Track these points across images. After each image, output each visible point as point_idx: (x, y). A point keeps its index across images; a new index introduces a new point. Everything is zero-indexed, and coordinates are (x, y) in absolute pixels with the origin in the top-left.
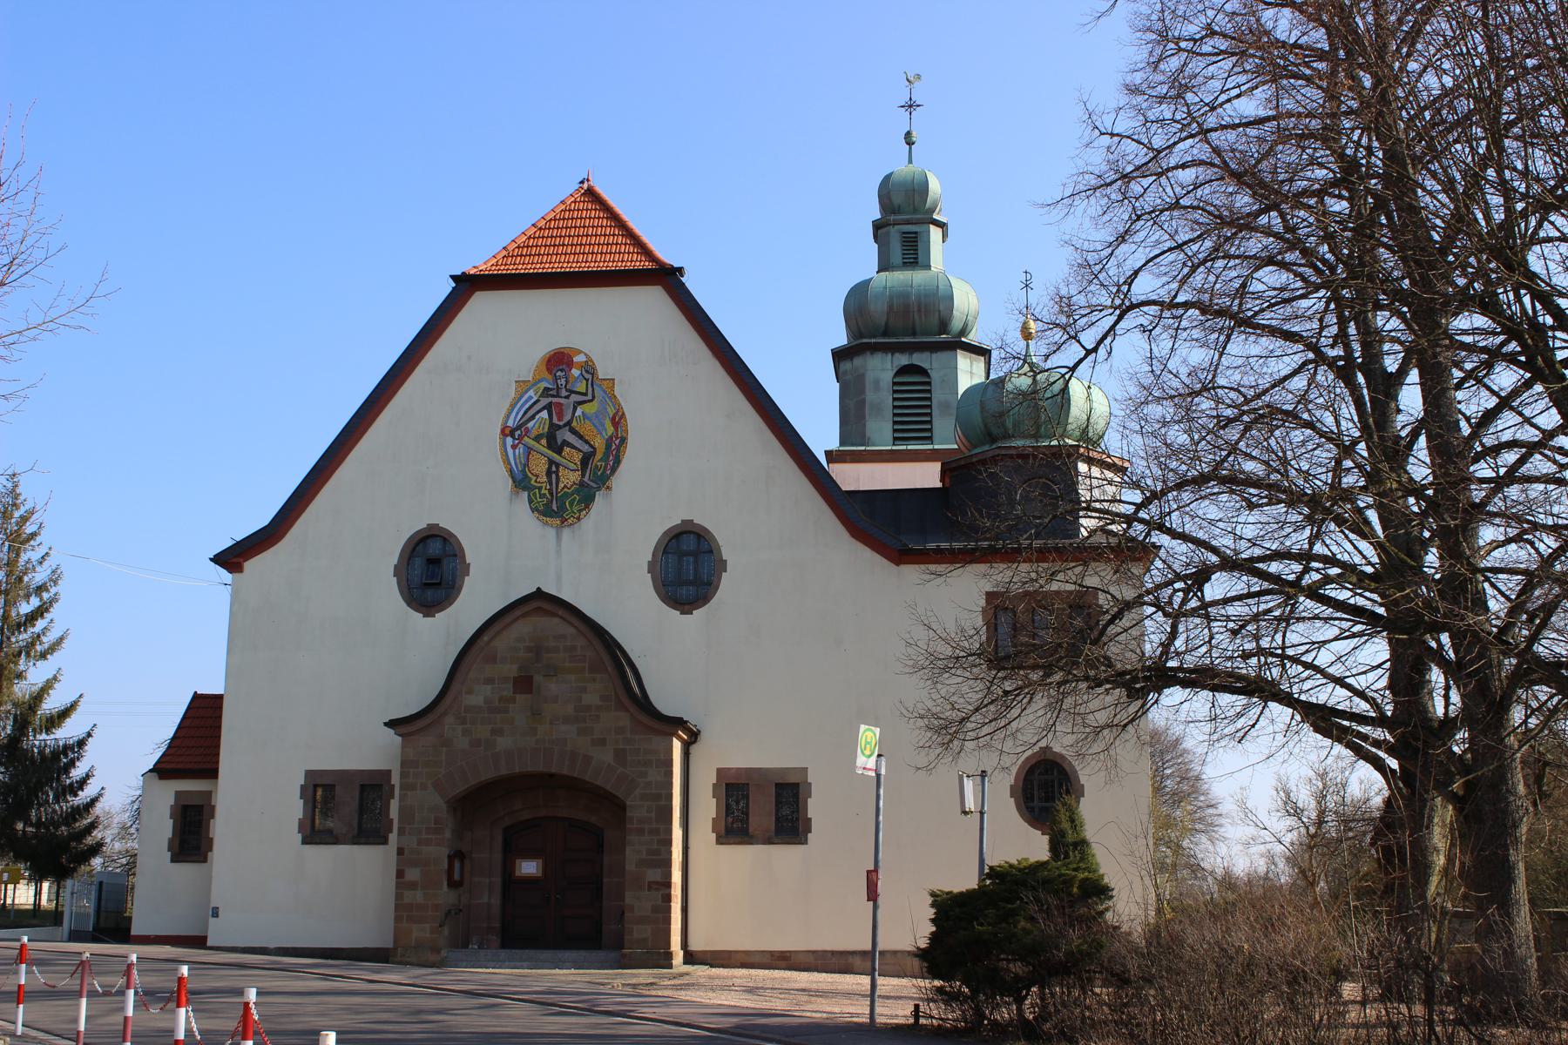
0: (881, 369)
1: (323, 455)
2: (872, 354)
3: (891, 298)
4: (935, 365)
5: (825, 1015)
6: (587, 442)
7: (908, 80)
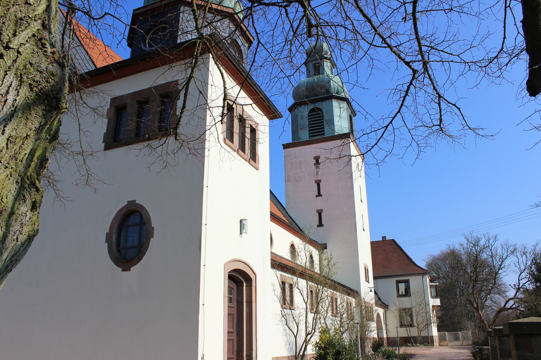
0: (304, 111)
1: (354, 208)
2: (300, 106)
3: (307, 85)
4: (324, 106)
5: (221, 68)
6: (182, 113)
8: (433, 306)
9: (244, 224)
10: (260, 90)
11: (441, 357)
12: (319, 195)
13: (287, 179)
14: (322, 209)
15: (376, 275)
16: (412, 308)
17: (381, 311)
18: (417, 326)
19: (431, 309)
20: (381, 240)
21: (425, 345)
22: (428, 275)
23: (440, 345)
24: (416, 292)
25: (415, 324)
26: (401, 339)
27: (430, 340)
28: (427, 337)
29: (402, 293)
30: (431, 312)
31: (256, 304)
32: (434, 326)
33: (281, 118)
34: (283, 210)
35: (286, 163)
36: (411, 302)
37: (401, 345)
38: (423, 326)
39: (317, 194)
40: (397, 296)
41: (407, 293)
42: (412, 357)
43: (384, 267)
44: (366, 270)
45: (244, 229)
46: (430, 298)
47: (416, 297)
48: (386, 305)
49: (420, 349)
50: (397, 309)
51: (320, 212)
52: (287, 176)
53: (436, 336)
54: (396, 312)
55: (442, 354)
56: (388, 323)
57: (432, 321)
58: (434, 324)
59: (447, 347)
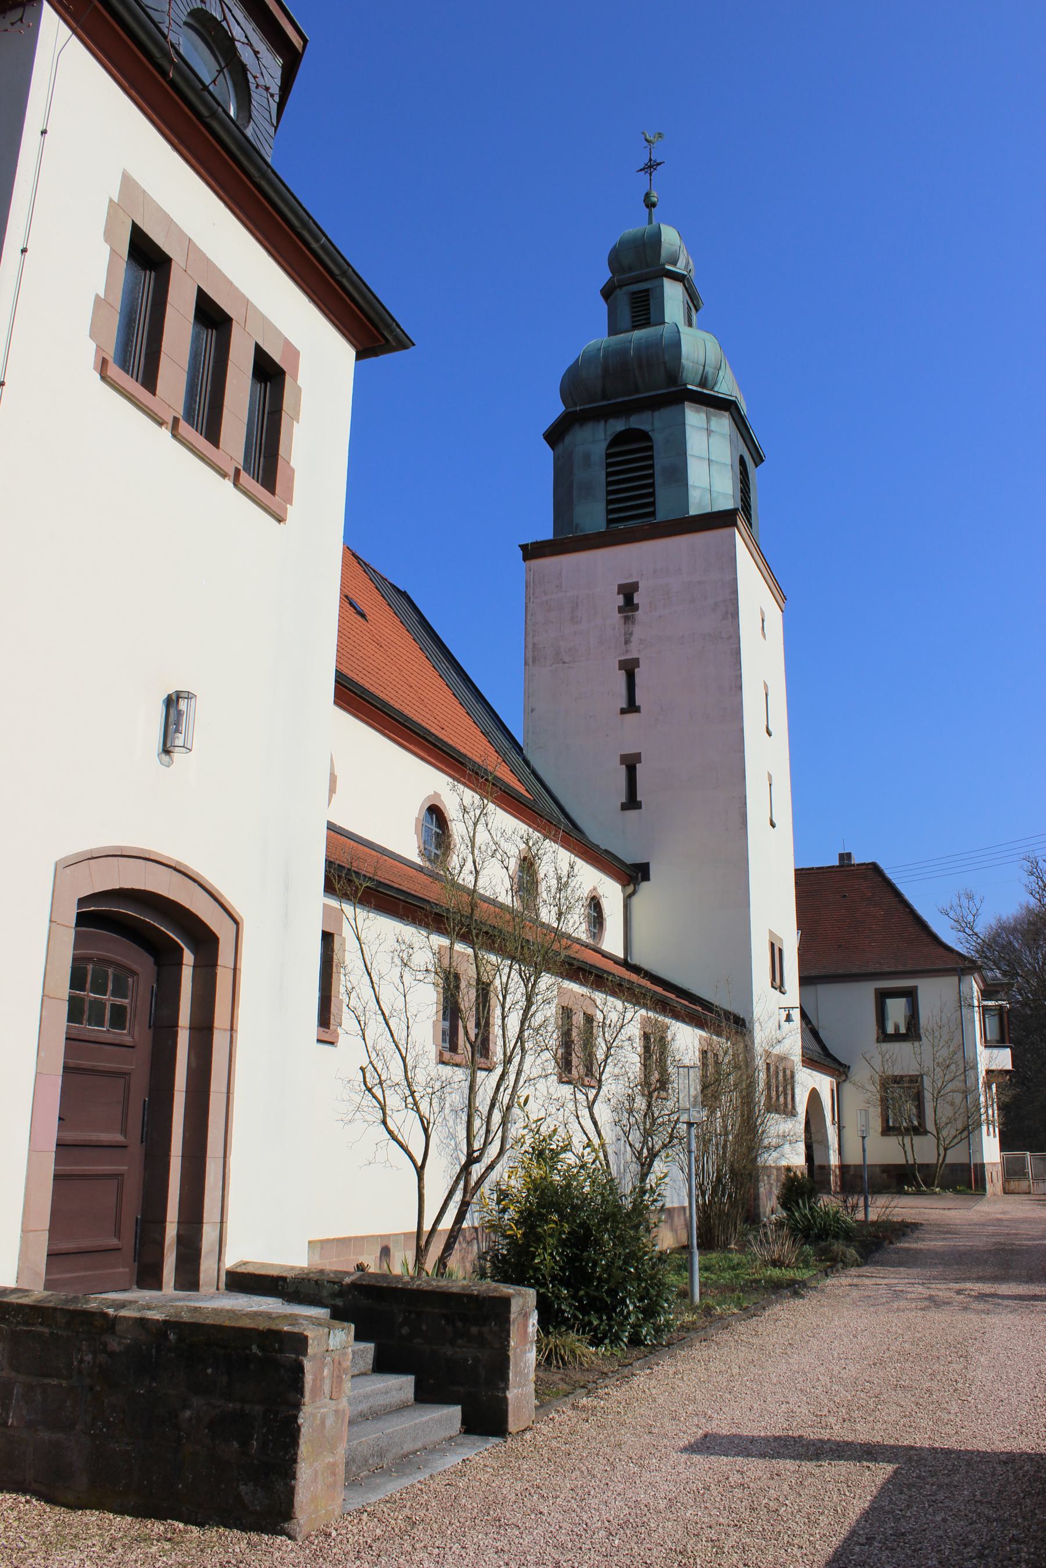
2: (581, 425)
3: (606, 357)
4: (657, 425)
7: (647, 140)
8: (989, 1072)
9: (179, 713)
10: (301, 212)
11: (998, 1235)
12: (632, 707)
13: (530, 654)
14: (640, 753)
16: (921, 1076)
17: (824, 1083)
18: (935, 1132)
19: (981, 1081)
20: (837, 863)
21: (959, 1192)
22: (976, 975)
23: (1006, 1192)
24: (936, 1028)
25: (930, 1126)
26: (883, 1172)
27: (976, 1175)
28: (965, 1168)
29: (897, 1027)
30: (981, 1089)
31: (231, 1036)
32: (988, 1134)
33: (405, 347)
34: (513, 755)
35: (531, 605)
36: (918, 1057)
37: (878, 1189)
38: (953, 1133)
39: (624, 706)
40: (878, 1038)
41: (912, 1032)
42: (904, 1235)
43: (839, 946)
44: (776, 954)
45: (177, 731)
46: (980, 1048)
47: (936, 1040)
48: (840, 1064)
49: (941, 1204)
50: (877, 1078)
51: (631, 764)
52: (530, 646)
53: (994, 1164)
54: (872, 1088)
55: (1007, 1223)
56: (847, 1121)
57: (983, 1117)
58: (991, 1127)
59: (1026, 1197)
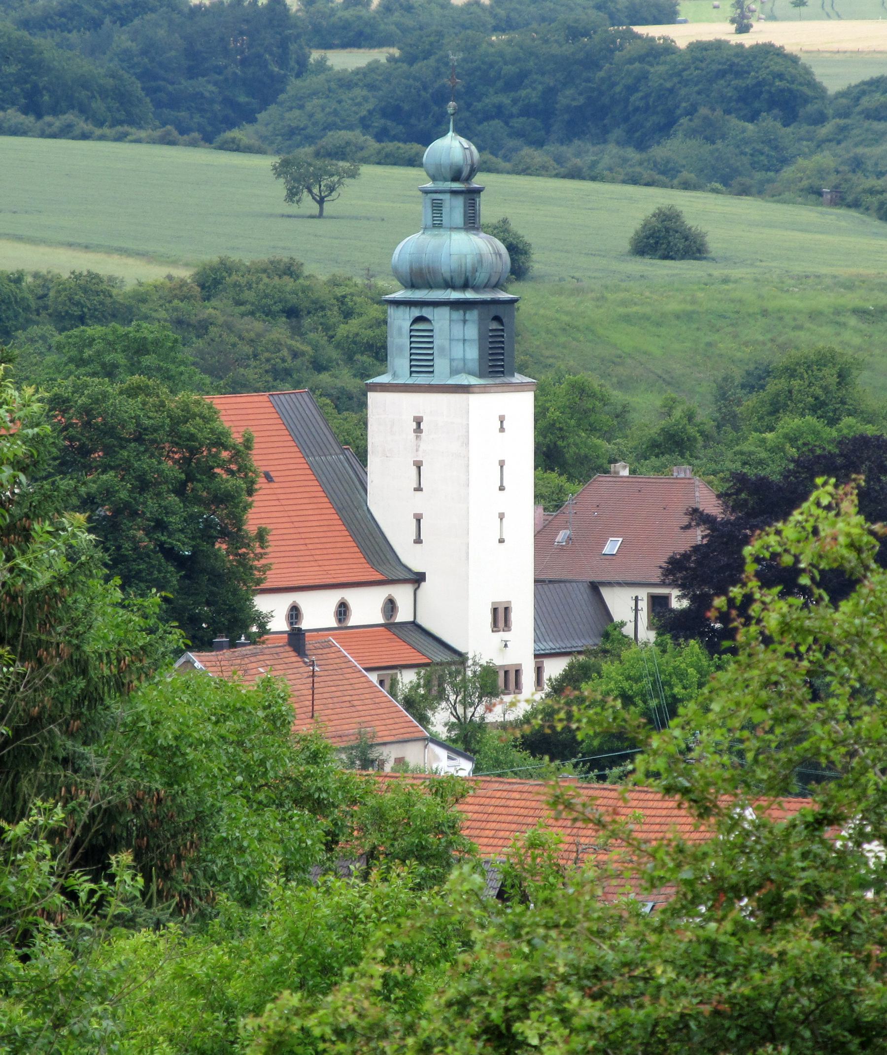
12: (419, 489)
15: (542, 577)
